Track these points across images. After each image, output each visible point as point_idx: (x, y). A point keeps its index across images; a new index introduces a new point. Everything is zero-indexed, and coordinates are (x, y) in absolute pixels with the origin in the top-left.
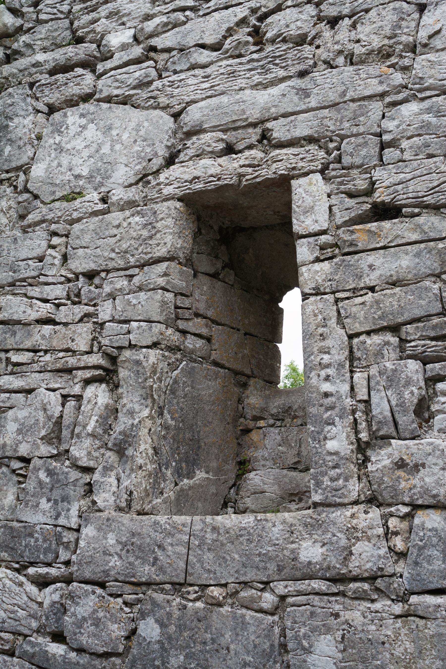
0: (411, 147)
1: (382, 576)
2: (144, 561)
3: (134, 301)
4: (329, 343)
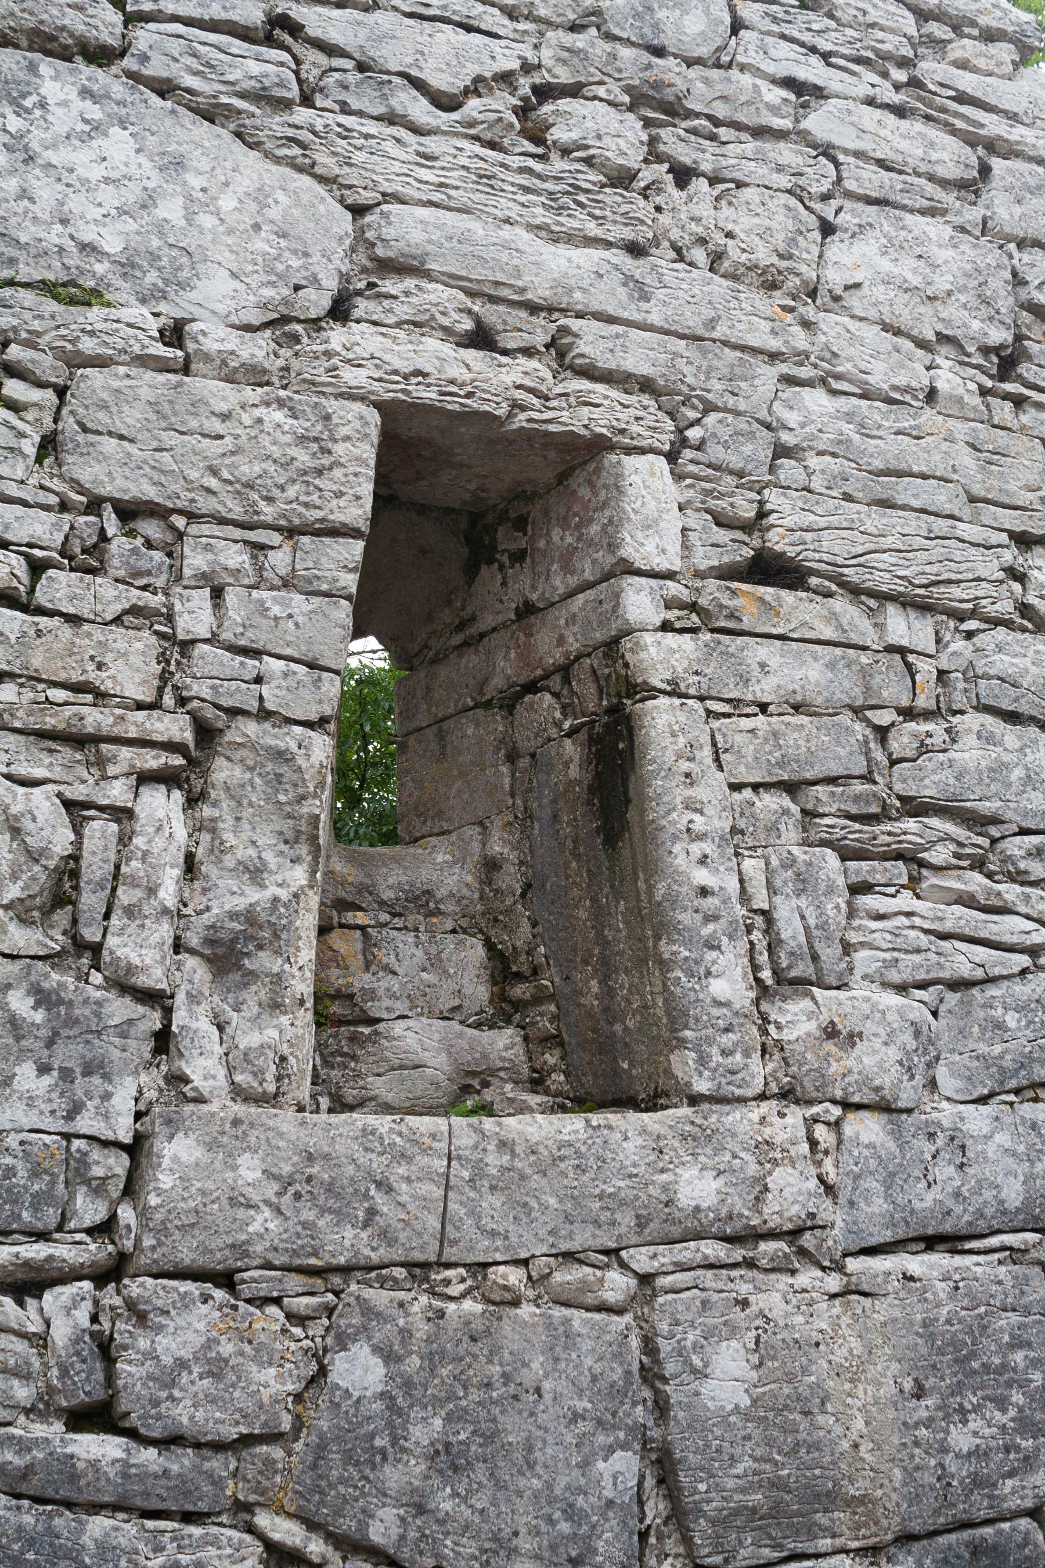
0: (823, 472)
1: (812, 1228)
2: (341, 1217)
3: (276, 610)
4: (699, 792)
